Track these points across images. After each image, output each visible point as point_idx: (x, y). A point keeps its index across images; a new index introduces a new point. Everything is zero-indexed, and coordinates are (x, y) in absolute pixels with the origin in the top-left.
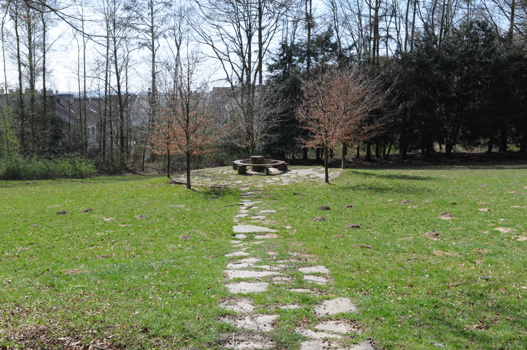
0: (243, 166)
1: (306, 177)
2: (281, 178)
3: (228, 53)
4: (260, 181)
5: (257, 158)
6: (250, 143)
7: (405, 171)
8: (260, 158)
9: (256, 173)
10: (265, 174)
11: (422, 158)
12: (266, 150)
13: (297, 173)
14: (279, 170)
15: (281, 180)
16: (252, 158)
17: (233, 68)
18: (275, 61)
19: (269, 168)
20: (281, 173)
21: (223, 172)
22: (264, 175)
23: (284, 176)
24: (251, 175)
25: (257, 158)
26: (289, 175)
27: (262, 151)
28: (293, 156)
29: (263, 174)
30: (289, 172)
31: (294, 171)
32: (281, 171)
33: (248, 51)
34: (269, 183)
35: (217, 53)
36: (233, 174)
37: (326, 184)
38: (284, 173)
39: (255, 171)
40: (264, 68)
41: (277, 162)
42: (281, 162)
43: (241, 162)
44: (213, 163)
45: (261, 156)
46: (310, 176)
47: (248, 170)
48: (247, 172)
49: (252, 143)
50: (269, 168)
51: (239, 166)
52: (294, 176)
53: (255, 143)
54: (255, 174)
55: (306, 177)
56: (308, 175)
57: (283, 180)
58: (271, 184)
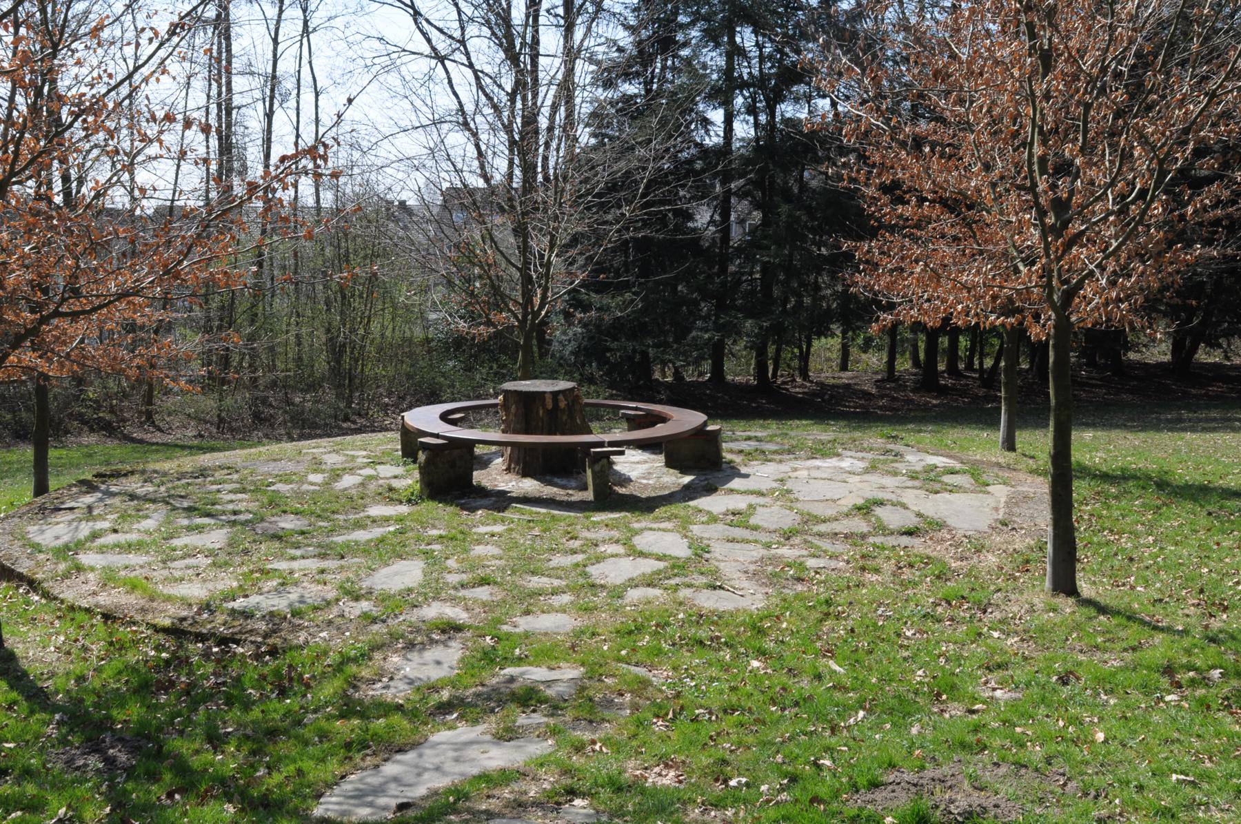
0: (453, 442)
1: (859, 525)
2: (696, 530)
3: (463, 29)
4: (558, 560)
5: (541, 395)
6: (516, 317)
7: (1135, 439)
8: (555, 394)
9: (530, 486)
10: (589, 495)
11: (1101, 380)
12: (586, 349)
13: (785, 495)
14: (670, 464)
15: (701, 551)
16: (507, 393)
17: (480, 87)
18: (620, 50)
19: (614, 458)
20: (688, 493)
21: (336, 475)
22: (582, 506)
23: (713, 519)
24: (500, 501)
25: (538, 396)
26: (740, 503)
27: (572, 353)
28: (677, 375)
29: (577, 496)
30: (736, 483)
31: (762, 474)
32: (684, 470)
33: (529, 39)
34: (617, 592)
35: (424, 34)
36: (390, 495)
37: (1067, 605)
38: (710, 490)
39: (525, 474)
40: (582, 70)
41: (663, 419)
42: (685, 420)
43: (444, 417)
44: (403, 398)
45: (563, 385)
46: (878, 511)
47: (484, 463)
48: (479, 477)
49: (525, 315)
50: (614, 458)
51: (425, 447)
52: (772, 516)
53: (536, 314)
54: (526, 500)
55: (859, 525)
56: (865, 509)
57: (718, 550)
58: (634, 595)
